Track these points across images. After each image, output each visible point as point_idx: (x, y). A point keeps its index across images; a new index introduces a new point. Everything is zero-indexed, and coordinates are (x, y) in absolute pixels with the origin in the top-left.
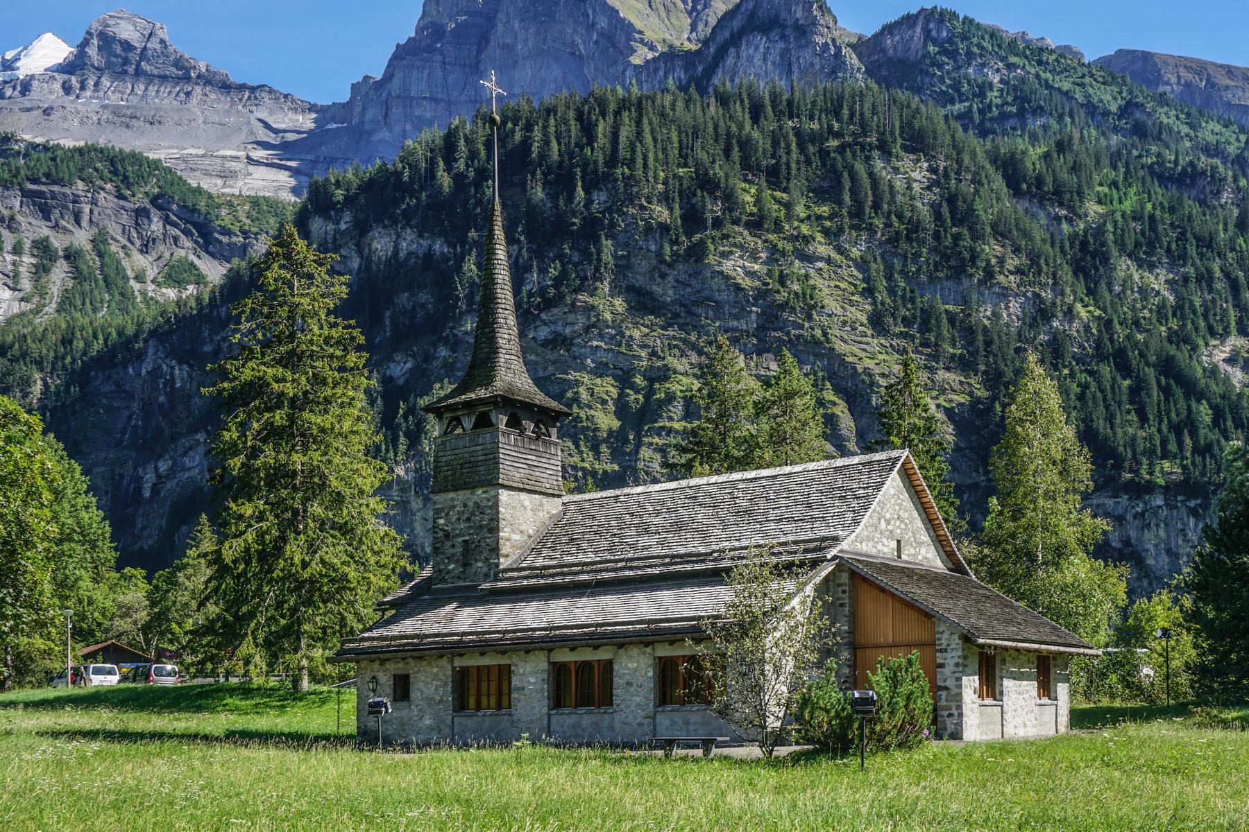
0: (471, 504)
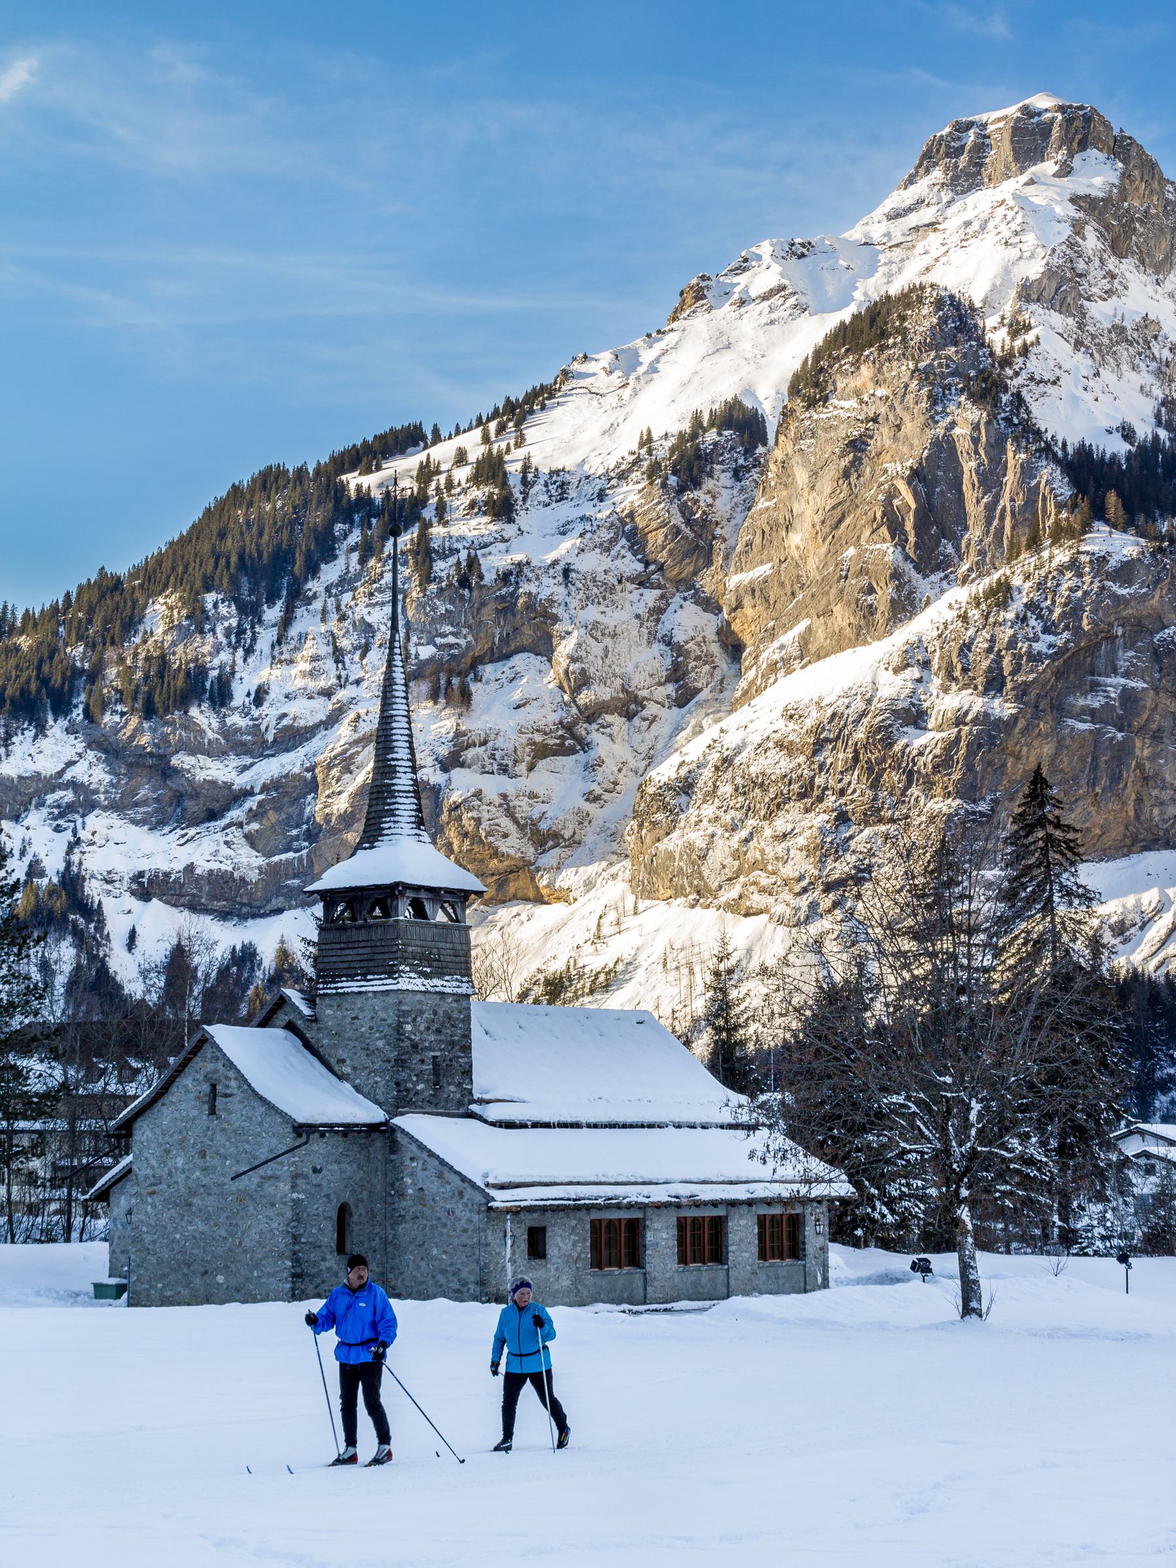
0: (441, 1012)
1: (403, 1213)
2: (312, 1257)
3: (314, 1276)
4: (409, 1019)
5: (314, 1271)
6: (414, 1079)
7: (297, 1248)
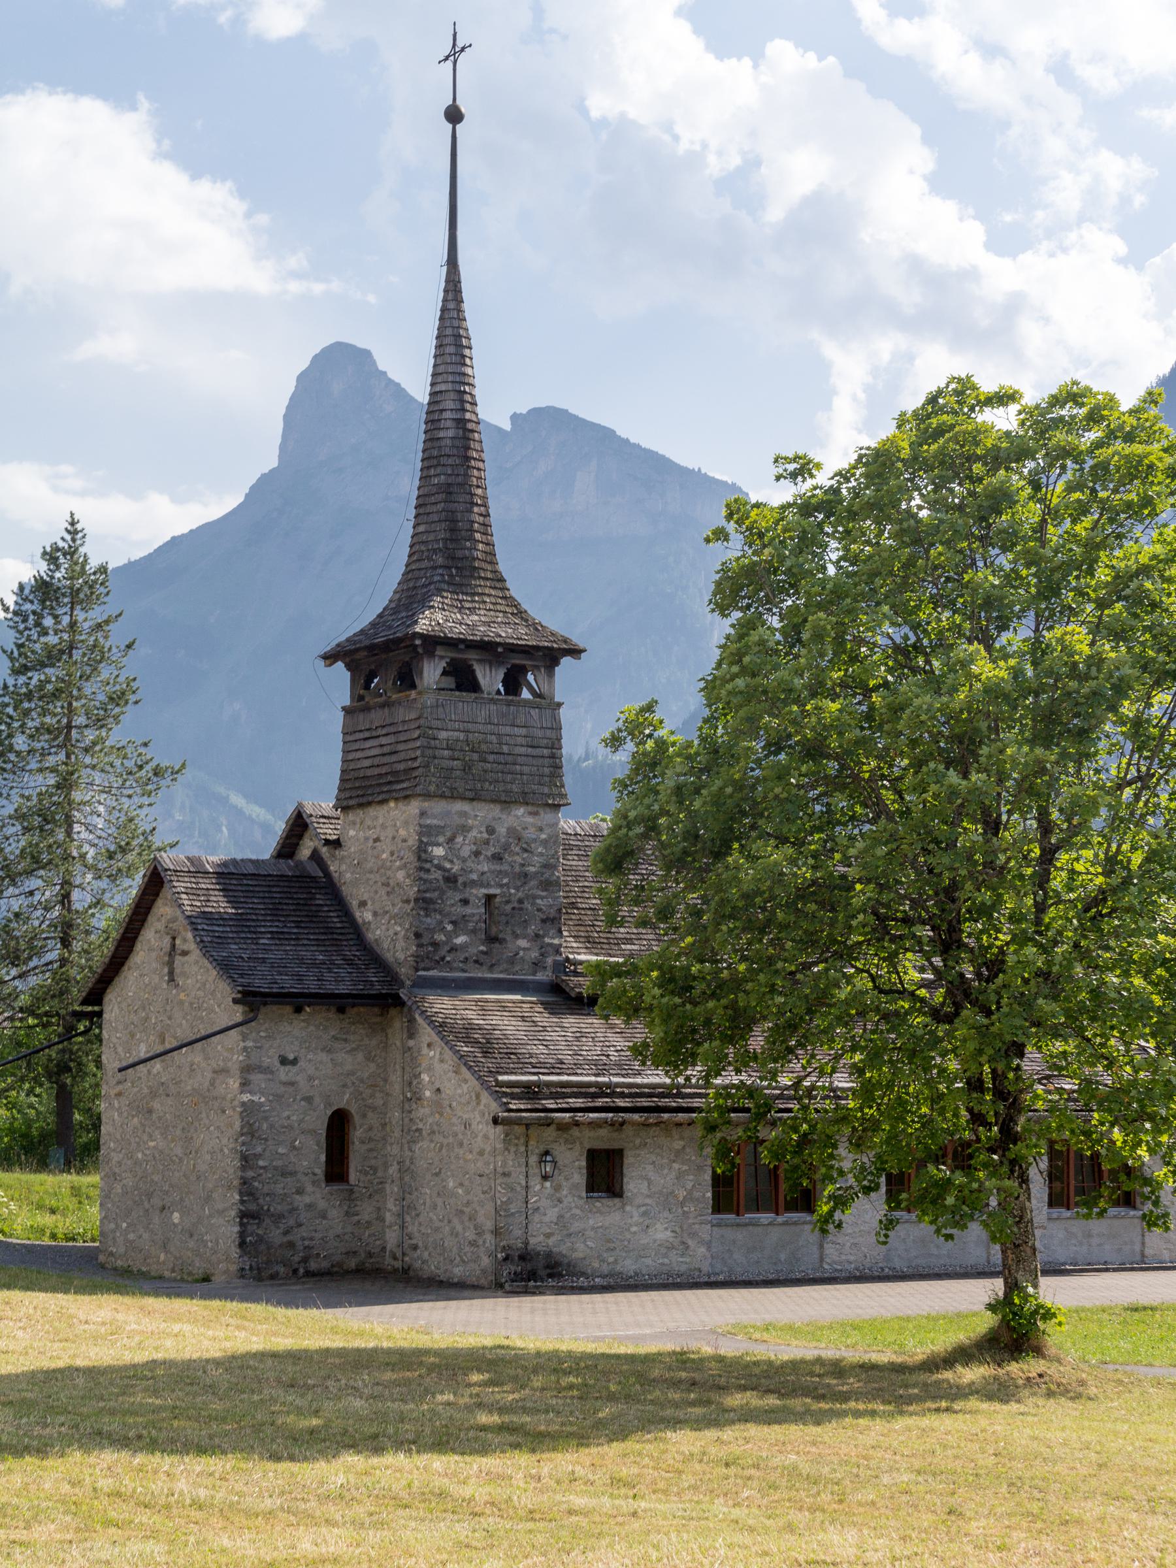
1: (420, 1126)
2: (279, 1189)
3: (281, 1216)
4: (441, 839)
5: (277, 1208)
6: (449, 927)
7: (250, 1174)
